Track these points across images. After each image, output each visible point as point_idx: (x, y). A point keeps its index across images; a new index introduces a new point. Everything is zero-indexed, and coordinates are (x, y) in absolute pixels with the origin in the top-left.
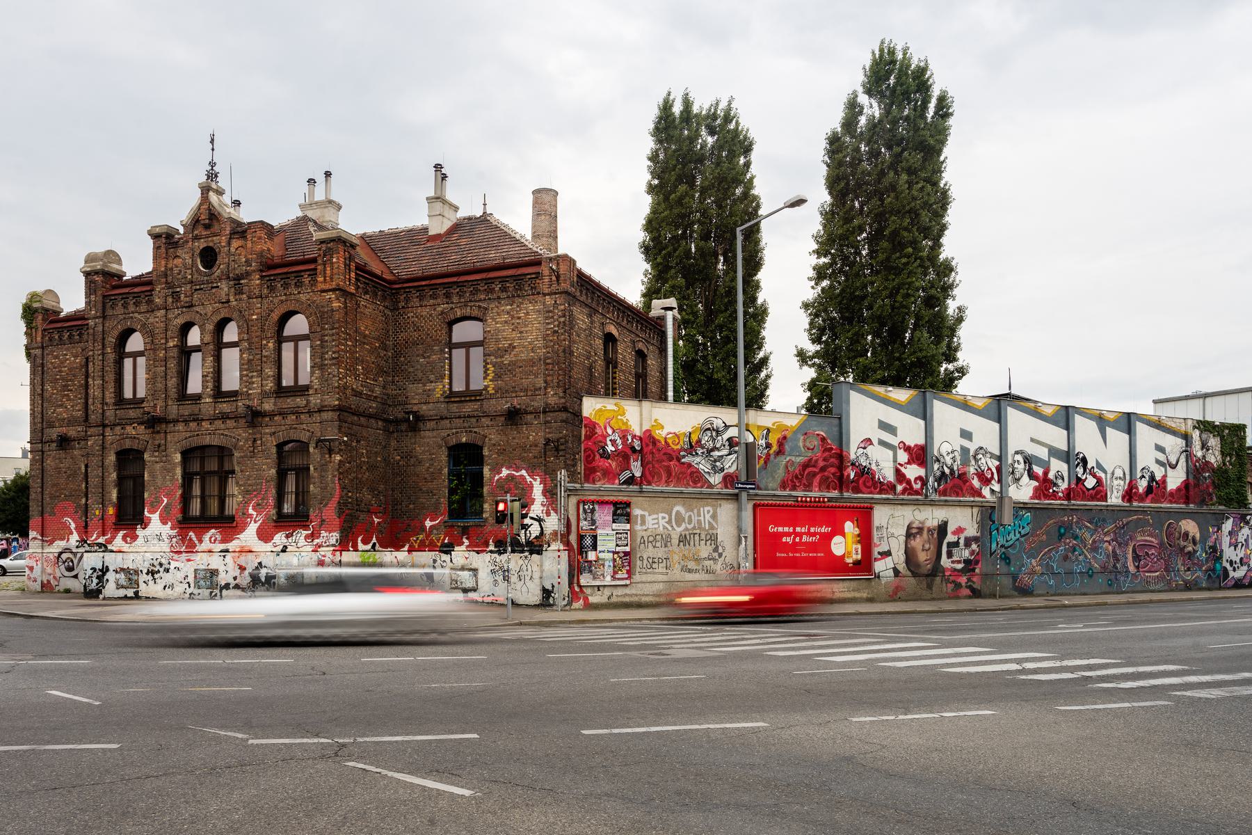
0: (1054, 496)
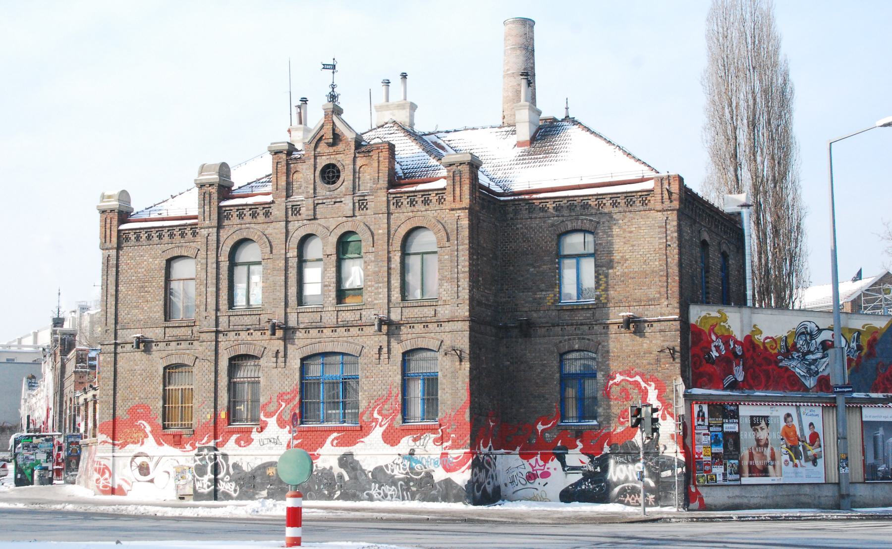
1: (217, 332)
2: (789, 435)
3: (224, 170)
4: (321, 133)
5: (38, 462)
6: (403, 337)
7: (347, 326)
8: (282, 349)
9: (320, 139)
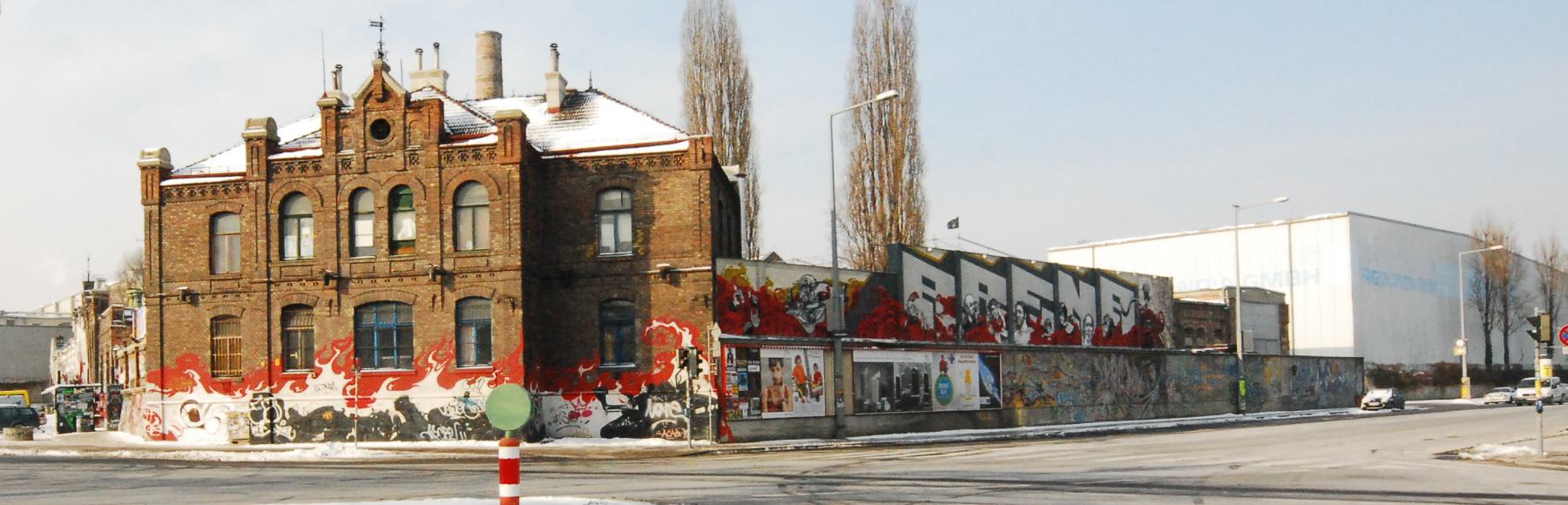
0: (1045, 341)
1: (269, 283)
2: (798, 373)
3: (271, 124)
5: (80, 411)
8: (335, 298)
9: (370, 95)
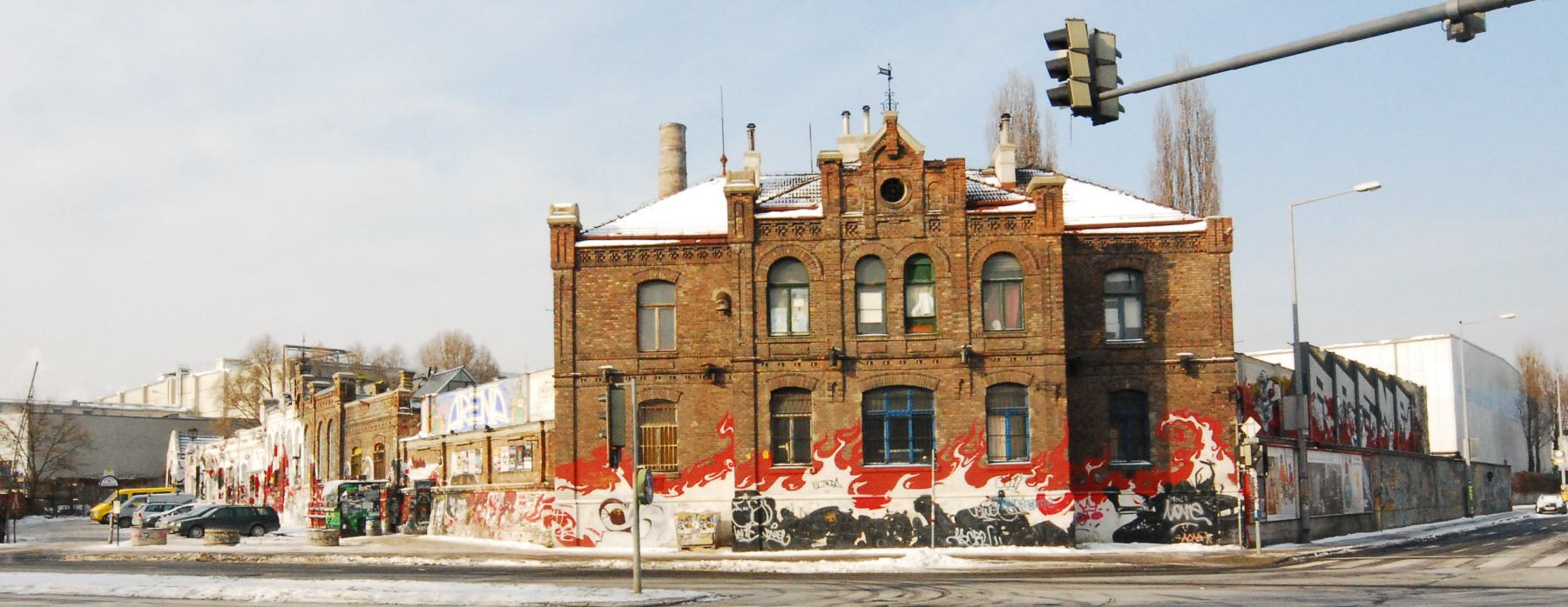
4: (884, 143)
6: (988, 370)
7: (918, 356)
